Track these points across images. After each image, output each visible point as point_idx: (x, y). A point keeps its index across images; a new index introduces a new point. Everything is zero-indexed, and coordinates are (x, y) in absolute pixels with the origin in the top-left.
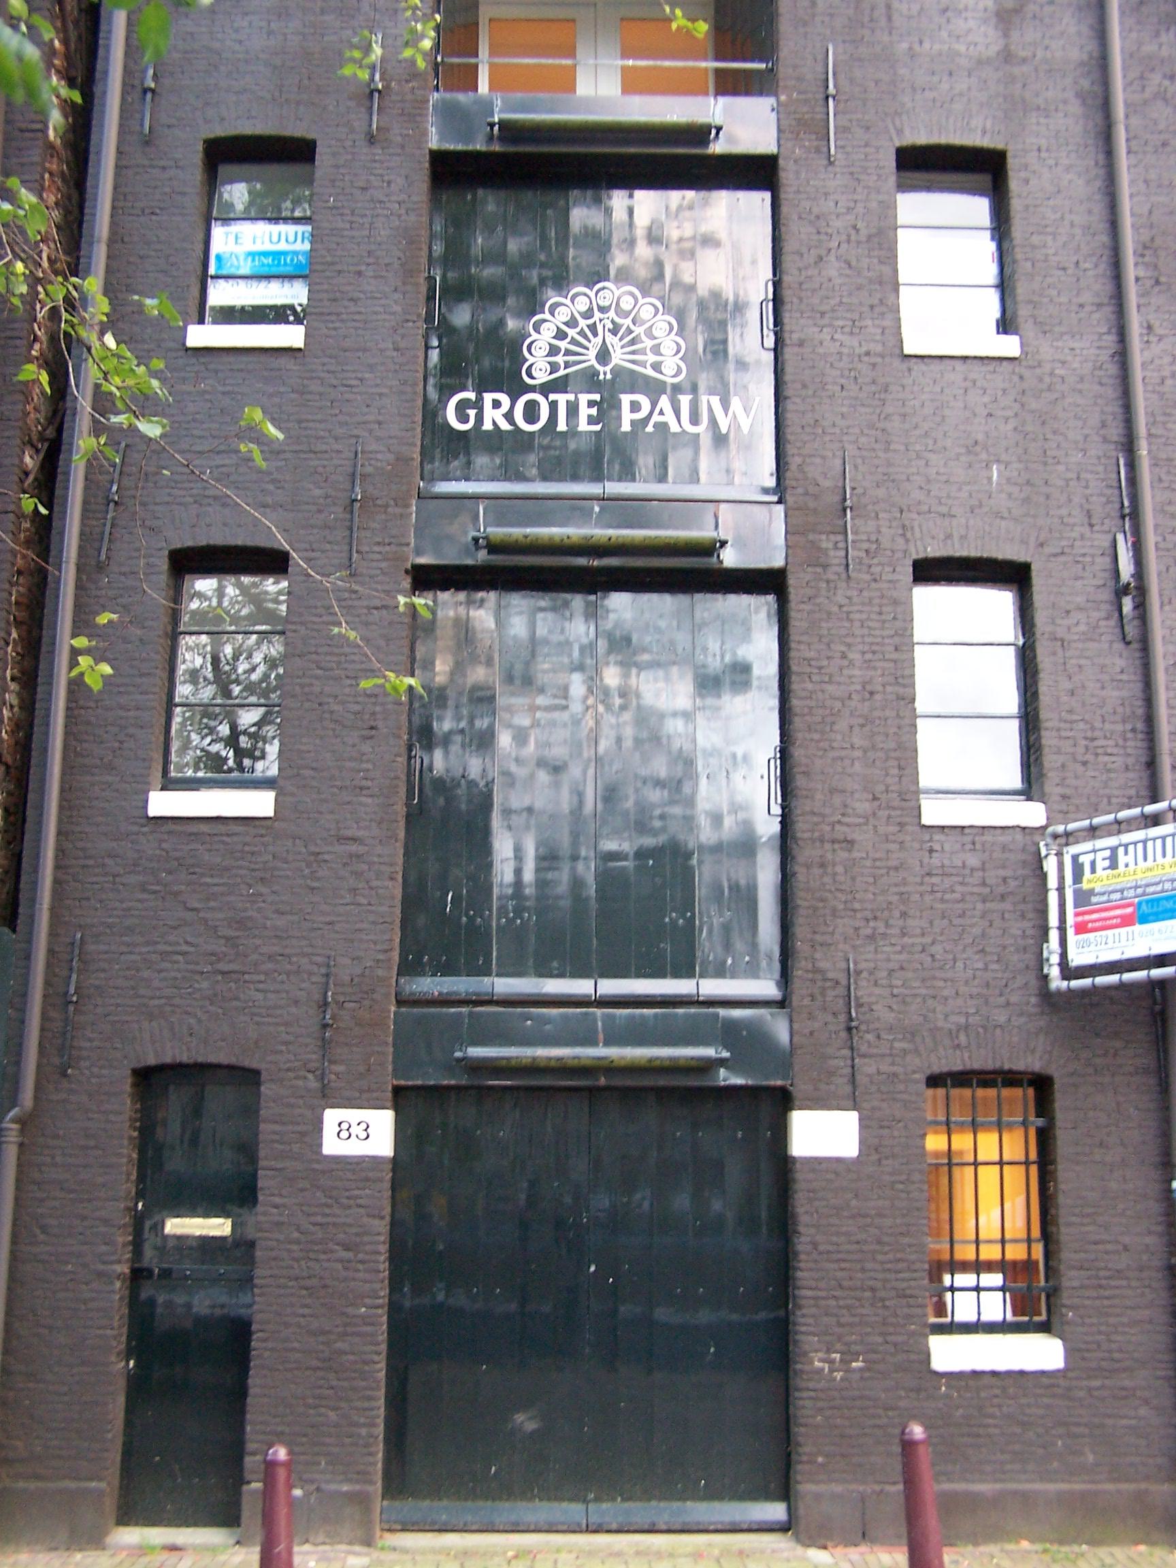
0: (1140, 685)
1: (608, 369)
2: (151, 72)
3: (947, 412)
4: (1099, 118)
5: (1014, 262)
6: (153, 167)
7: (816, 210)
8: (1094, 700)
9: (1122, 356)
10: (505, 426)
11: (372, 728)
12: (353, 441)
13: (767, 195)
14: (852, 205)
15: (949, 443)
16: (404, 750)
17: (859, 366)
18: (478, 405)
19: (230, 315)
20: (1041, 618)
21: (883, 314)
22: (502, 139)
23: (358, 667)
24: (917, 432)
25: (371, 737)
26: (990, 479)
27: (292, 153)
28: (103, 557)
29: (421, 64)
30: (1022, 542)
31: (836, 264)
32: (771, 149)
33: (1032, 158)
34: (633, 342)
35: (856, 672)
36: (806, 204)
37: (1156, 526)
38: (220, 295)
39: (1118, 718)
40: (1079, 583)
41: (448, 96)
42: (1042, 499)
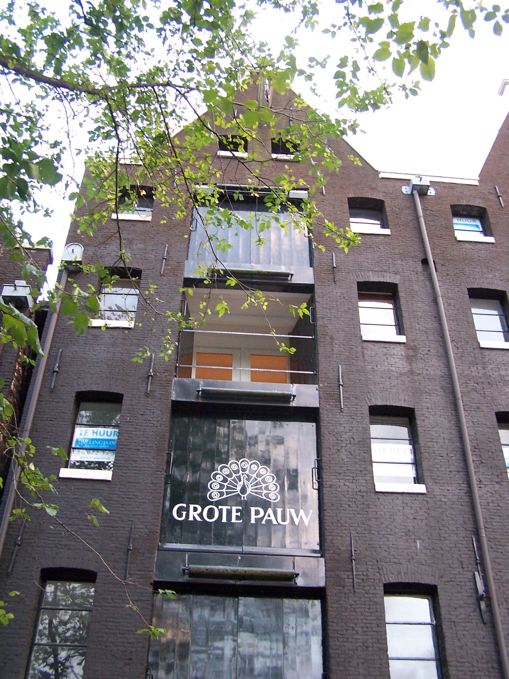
0: (492, 645)
1: (245, 495)
2: (57, 365)
3: (396, 517)
4: (451, 397)
5: (421, 453)
6: (53, 401)
7: (336, 430)
8: (472, 652)
9: (470, 493)
10: (198, 519)
11: (130, 659)
12: (130, 523)
13: (314, 424)
14: (351, 428)
15: (397, 531)
16: (144, 671)
17: (356, 497)
18: (187, 510)
19: (82, 465)
20: (443, 611)
21: (366, 474)
22: (202, 397)
23: (126, 629)
24: (383, 526)
25: (129, 664)
26: (416, 547)
27: (115, 399)
28: (10, 570)
29: (167, 359)
30: (433, 576)
31: (345, 453)
32: (317, 405)
33: (425, 412)
34: (257, 484)
35: (360, 637)
36: (332, 428)
37: (492, 568)
38: (76, 456)
39: (484, 661)
40: (459, 595)
41: (180, 379)
42: (440, 556)
